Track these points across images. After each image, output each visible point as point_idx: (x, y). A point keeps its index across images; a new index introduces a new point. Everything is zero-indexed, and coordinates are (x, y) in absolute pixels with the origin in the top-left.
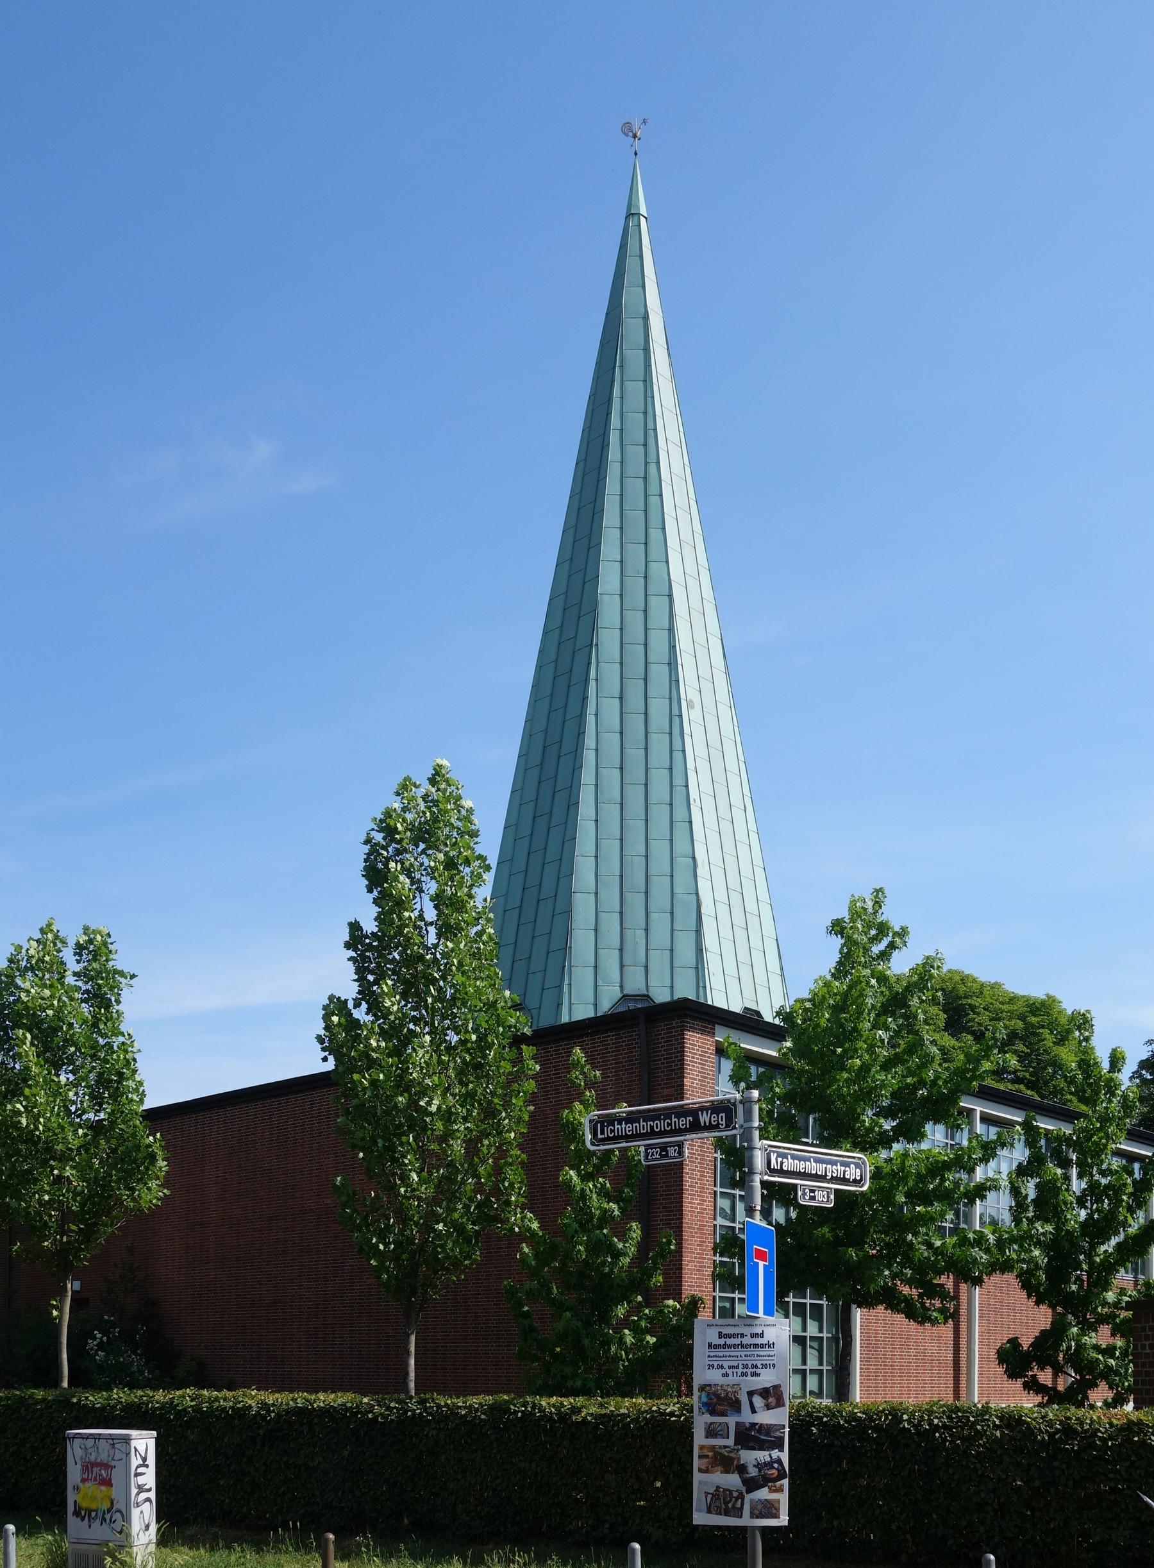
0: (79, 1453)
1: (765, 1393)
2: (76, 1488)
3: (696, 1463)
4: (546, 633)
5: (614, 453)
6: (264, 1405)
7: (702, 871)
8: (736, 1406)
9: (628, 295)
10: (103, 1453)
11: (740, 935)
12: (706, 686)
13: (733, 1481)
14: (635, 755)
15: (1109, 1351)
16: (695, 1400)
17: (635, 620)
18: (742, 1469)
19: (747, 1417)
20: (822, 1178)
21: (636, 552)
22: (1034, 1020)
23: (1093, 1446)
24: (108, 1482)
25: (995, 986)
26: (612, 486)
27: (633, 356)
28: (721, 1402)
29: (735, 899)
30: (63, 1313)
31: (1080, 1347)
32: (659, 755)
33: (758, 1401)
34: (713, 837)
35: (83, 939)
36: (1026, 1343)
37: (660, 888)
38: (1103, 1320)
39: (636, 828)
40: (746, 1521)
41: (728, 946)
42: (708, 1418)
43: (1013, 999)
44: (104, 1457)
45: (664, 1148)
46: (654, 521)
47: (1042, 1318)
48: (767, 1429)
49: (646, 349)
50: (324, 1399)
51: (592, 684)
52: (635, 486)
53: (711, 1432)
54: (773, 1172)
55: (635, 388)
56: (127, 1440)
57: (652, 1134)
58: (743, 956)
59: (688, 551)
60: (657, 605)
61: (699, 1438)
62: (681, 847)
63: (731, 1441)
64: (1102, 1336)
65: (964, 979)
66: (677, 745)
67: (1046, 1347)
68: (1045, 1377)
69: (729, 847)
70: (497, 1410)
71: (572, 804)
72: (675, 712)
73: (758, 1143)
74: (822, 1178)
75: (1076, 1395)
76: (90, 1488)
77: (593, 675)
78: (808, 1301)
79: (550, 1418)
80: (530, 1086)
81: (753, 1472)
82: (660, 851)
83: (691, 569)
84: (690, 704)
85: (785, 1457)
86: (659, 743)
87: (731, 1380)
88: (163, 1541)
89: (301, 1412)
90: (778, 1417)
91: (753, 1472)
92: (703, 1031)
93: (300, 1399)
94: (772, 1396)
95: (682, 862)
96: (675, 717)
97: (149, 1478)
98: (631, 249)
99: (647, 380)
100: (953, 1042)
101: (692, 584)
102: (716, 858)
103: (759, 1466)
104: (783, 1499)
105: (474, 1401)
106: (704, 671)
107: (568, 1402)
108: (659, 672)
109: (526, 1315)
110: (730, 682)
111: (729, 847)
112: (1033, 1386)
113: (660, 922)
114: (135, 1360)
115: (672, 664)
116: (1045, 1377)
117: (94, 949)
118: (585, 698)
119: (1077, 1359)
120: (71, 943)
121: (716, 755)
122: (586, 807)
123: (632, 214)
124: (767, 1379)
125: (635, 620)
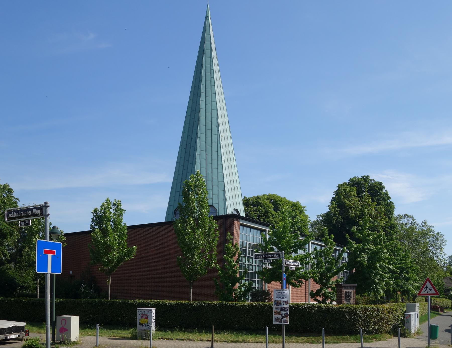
0: (140, 312)
1: (285, 302)
2: (140, 319)
3: (274, 314)
4: (186, 116)
5: (203, 74)
6: (169, 303)
7: (225, 176)
8: (281, 304)
9: (207, 36)
10: (146, 312)
11: (233, 191)
12: (225, 132)
13: (280, 316)
14: (209, 148)
15: (330, 293)
16: (273, 303)
17: (209, 115)
18: (282, 315)
19: (282, 306)
20: (293, 265)
21: (209, 99)
22: (294, 208)
23: (333, 311)
24: (147, 318)
25: (284, 198)
26: (203, 83)
27: (208, 51)
28: (278, 303)
29: (232, 182)
30: (109, 283)
31: (325, 292)
32: (215, 149)
33: (284, 303)
34: (227, 168)
35: (115, 202)
36: (315, 292)
37: (215, 180)
38: (329, 287)
39: (209, 165)
40: (282, 323)
41: (230, 194)
42: (276, 306)
43: (289, 202)
44: (146, 313)
45: (267, 260)
46: (213, 92)
47: (318, 287)
48: (286, 308)
49: (211, 50)
50: (182, 302)
51: (199, 130)
52: (208, 83)
53: (276, 308)
54: (286, 265)
55: (208, 59)
56: (151, 310)
57: (265, 258)
58: (234, 197)
59: (221, 99)
60: (214, 112)
61: (274, 309)
62: (220, 170)
63: (280, 310)
64: (329, 290)
65: (277, 197)
66: (219, 146)
67: (318, 292)
68: (318, 298)
69: (230, 171)
70: (219, 304)
71: (194, 159)
72: (218, 138)
73: (284, 260)
74: (293, 265)
75: (323, 302)
76: (143, 319)
77: (199, 128)
78: (253, 279)
79: (231, 306)
80: (218, 239)
81: (283, 315)
82: (215, 171)
83: (221, 103)
84: (222, 136)
85: (288, 313)
86: (215, 145)
87: (280, 300)
88: (157, 330)
89: (178, 304)
90: (287, 306)
91: (283, 315)
92: (237, 221)
93: (177, 302)
94: (287, 302)
95: (220, 174)
96: (218, 139)
97: (154, 318)
98: (207, 25)
99: (211, 57)
100: (275, 213)
101: (222, 107)
102: (228, 173)
103: (284, 314)
104: (288, 319)
105: (215, 302)
106: (225, 128)
107: (234, 303)
108: (214, 128)
109: (218, 285)
110: (230, 130)
111: (230, 171)
112: (315, 300)
113: (215, 188)
114: (92, 291)
115: (218, 126)
116: (318, 298)
117: (117, 205)
118: (197, 134)
119: (324, 295)
120: (112, 203)
121: (227, 148)
122: (198, 160)
123: (207, 17)
124: (286, 300)
125: (209, 115)
